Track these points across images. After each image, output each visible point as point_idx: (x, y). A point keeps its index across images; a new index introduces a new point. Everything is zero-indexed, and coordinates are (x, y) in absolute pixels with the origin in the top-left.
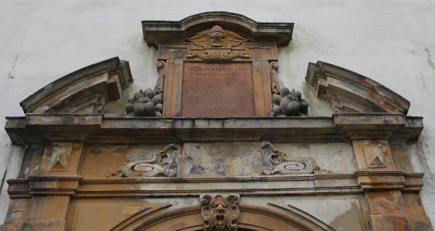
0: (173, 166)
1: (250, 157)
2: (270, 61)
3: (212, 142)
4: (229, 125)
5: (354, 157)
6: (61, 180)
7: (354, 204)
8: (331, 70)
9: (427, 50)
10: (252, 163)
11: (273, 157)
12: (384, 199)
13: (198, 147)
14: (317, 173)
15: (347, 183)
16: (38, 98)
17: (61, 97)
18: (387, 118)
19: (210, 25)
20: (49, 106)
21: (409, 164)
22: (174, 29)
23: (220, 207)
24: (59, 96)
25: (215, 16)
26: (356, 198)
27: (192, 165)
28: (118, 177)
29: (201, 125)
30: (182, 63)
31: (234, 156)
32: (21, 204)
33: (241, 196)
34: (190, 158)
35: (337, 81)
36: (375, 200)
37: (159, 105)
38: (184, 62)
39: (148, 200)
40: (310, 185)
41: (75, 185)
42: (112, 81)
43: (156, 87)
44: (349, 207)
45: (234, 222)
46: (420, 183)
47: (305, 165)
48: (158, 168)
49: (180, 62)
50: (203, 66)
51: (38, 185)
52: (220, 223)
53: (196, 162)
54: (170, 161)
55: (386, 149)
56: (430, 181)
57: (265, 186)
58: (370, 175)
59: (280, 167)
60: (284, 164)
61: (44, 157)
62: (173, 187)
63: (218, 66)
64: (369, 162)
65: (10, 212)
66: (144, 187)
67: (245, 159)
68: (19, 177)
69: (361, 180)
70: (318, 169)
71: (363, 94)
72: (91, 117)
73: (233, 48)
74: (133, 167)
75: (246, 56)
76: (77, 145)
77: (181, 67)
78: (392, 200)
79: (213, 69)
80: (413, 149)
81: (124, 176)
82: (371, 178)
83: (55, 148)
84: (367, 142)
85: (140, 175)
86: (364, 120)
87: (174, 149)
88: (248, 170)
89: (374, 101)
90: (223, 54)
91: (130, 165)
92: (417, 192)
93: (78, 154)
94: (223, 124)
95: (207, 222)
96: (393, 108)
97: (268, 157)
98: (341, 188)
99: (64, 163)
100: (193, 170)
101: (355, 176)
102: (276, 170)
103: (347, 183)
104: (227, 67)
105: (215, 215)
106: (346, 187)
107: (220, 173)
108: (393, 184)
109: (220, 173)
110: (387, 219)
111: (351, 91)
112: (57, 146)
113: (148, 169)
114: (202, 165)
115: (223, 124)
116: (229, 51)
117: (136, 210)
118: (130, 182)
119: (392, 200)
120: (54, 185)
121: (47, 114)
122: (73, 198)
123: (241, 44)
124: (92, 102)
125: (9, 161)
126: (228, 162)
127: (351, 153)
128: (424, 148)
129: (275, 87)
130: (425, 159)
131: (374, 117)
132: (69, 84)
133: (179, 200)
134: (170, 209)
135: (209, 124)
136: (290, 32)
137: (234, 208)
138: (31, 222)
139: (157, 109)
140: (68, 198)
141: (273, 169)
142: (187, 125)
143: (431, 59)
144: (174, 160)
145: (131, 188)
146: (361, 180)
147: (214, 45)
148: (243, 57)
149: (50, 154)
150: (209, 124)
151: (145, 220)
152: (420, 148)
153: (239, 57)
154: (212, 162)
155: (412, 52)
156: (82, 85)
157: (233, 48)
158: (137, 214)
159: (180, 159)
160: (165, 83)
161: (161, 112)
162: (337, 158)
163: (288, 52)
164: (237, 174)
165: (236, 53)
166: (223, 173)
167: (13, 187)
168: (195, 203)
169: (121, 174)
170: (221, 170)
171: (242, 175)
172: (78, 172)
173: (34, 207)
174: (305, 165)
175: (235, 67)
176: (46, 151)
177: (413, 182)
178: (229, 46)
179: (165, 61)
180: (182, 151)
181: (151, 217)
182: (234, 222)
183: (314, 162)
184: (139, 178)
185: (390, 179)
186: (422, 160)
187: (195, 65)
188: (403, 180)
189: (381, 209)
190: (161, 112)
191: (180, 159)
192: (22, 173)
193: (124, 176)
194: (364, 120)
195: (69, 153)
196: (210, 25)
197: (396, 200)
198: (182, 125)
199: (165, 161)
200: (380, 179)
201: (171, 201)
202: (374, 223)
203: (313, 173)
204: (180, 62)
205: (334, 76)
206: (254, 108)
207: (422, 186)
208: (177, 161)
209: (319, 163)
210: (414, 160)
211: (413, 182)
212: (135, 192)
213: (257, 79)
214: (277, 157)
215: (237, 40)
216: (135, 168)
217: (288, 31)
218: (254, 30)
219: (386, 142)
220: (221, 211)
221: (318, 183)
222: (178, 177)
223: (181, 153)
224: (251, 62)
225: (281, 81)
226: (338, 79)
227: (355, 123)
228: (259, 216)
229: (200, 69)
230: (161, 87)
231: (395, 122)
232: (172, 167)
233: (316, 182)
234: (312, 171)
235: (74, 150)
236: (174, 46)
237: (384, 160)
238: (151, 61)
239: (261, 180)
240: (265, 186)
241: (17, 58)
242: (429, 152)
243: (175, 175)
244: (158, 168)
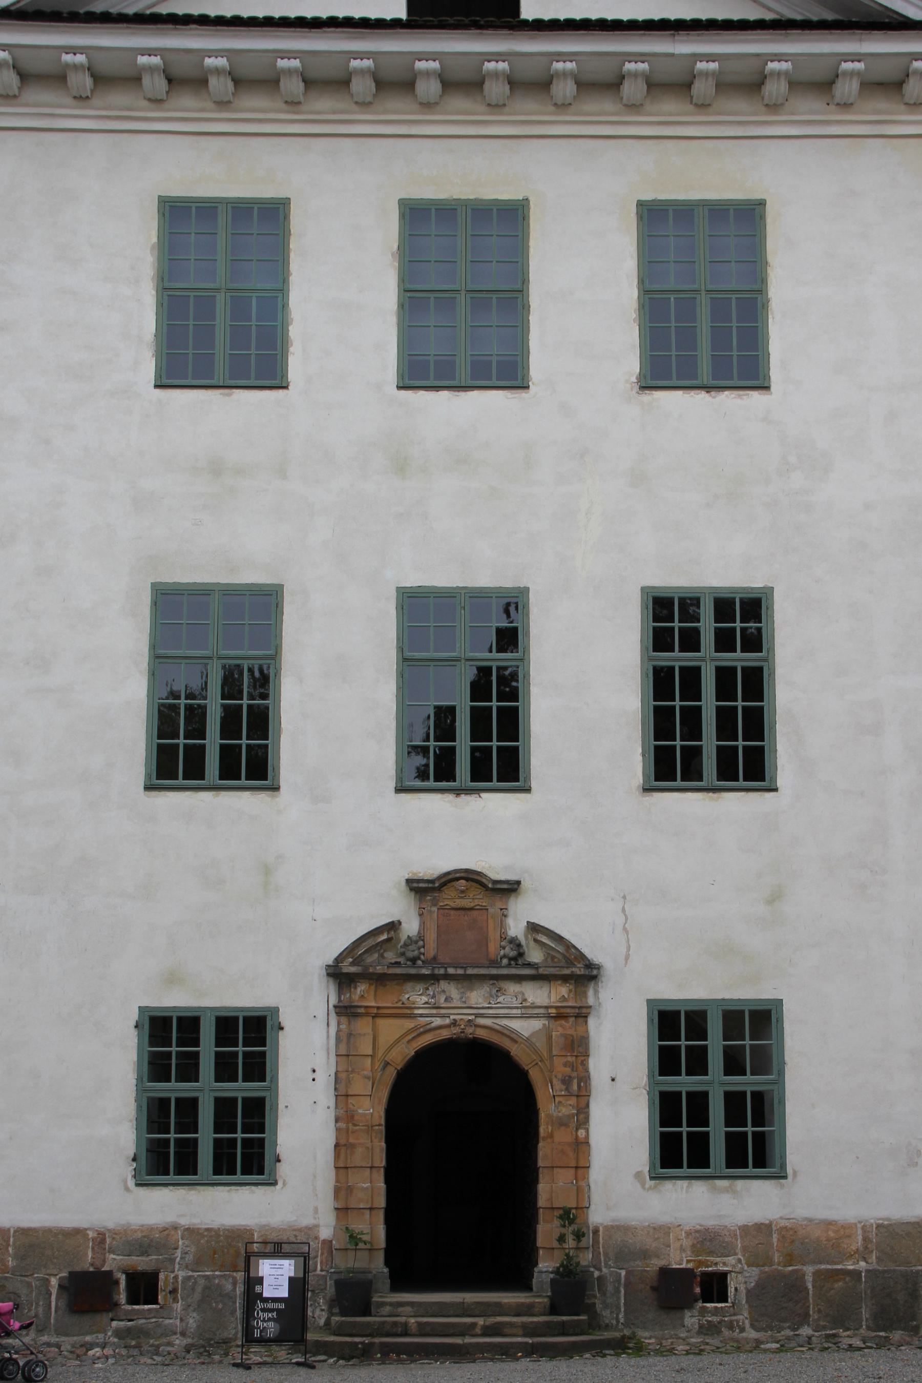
0: (433, 997)
1: (483, 990)
2: (501, 909)
3: (458, 980)
4: (470, 971)
5: (550, 992)
6: (366, 1007)
7: (544, 1025)
8: (541, 929)
9: (624, 897)
10: (484, 995)
11: (497, 991)
12: (563, 1022)
13: (449, 983)
14: (524, 1004)
15: (542, 1011)
16: (345, 953)
17: (358, 952)
18: (574, 969)
19: (458, 879)
20: (352, 958)
21: (586, 997)
22: (430, 885)
23: (462, 1027)
24: (357, 950)
25: (460, 873)
26: (547, 1020)
27: (445, 996)
28: (399, 1005)
29: (451, 971)
30: (436, 910)
31: (472, 990)
32: (344, 1019)
33: (476, 1017)
34: (444, 991)
35: (545, 937)
36: (558, 1022)
37: (422, 950)
38: (438, 909)
39: (419, 1018)
40: (519, 1011)
41: (375, 1011)
42: (390, 936)
43: (419, 932)
44: (541, 1026)
45: (470, 1034)
46: (588, 1012)
47: (517, 998)
48: (425, 999)
49: (435, 909)
50: (452, 912)
51: (353, 1010)
52: (462, 1035)
53: (448, 994)
54: (432, 993)
55: (571, 987)
56: (597, 1008)
57: (491, 1011)
58: (556, 1007)
59: (501, 999)
60: (504, 997)
61: (352, 990)
62: (434, 1011)
63: (463, 912)
64: (558, 998)
65: (339, 1024)
66: (416, 1012)
67: (479, 992)
68: (339, 1002)
69: (550, 1011)
70: (525, 1000)
71: (560, 949)
72: (380, 967)
73: (475, 897)
74: (409, 998)
75: (484, 904)
76: (371, 982)
77: (436, 914)
78: (568, 1022)
79: (459, 915)
80: (592, 985)
81: (403, 1004)
82: (557, 1010)
83: (358, 984)
84: (559, 982)
85: (414, 1004)
86: (557, 971)
87: (433, 984)
88: (480, 1000)
89: (568, 955)
90: (466, 903)
91: (407, 996)
92: (586, 1017)
93: (373, 987)
94: (465, 971)
95: (455, 1034)
96: (579, 963)
97: (494, 991)
98: (538, 1014)
99: (366, 995)
100: (446, 1000)
101: (547, 1007)
102: (498, 1001)
103: (542, 1011)
104: (469, 913)
105: (460, 1031)
106: (541, 1014)
107: (463, 1002)
108: (570, 1013)
109: (463, 1002)
110: (562, 1035)
111: (554, 946)
112: (359, 982)
113: (418, 1000)
114: (452, 996)
115: (465, 971)
116: (471, 900)
117: (412, 1025)
118: (407, 1008)
119: (568, 1022)
120: (362, 1010)
121: (353, 964)
122: (373, 1017)
123: (481, 893)
124: (377, 949)
125: (328, 986)
126: (468, 994)
127: (548, 989)
128: (600, 984)
129: (504, 933)
130: (598, 992)
131: (565, 969)
132: (363, 942)
133: (438, 1019)
134: (433, 1025)
135: (456, 971)
136: (502, 965)
137: (471, 1026)
138: (353, 1032)
139: (421, 953)
140: (371, 1018)
141: (497, 1000)
142: (442, 971)
143: (625, 906)
144: (434, 992)
145: (409, 1012)
146: (550, 1011)
147: (460, 895)
148: (482, 906)
149: (355, 988)
150: (456, 971)
151: (418, 1032)
152: (597, 984)
153: (478, 905)
154: (458, 994)
155: (612, 900)
156: (371, 942)
157: (475, 897)
158: (413, 1028)
159: (438, 992)
160: (425, 930)
161: (424, 954)
162: (539, 992)
163: (517, 897)
164: (473, 1003)
165: (476, 902)
166: (465, 1002)
167: (338, 1009)
168: (447, 1021)
169: (401, 1003)
170: (464, 999)
171: (477, 1004)
172: (375, 999)
173: (353, 1023)
174: (517, 998)
175: (475, 913)
176: (352, 985)
177: (584, 1011)
178: (471, 896)
179: (424, 909)
180: (438, 986)
181: (422, 1030)
182: (470, 1034)
183: (523, 994)
184: (413, 1006)
185: (568, 1010)
186: (596, 992)
187: (446, 911)
188: (577, 1011)
189: (560, 1029)
190: (424, 954)
191: (438, 992)
192: (340, 1001)
193: (403, 1004)
194: (557, 971)
195: (367, 988)
196: (458, 879)
197: (571, 1023)
198: (439, 971)
199: (428, 992)
200: (562, 1010)
201: (433, 1019)
202: (553, 1037)
203: (521, 1004)
204: (435, 909)
205: (543, 933)
206: (487, 950)
207: (589, 1013)
208: (436, 993)
209: (526, 996)
210: (591, 993)
211: (584, 1011)
212: (411, 1014)
213: (491, 922)
214: (499, 990)
215: (477, 890)
216: (410, 999)
217: (516, 886)
218: (490, 886)
219: (573, 982)
220: (463, 1029)
221: (524, 1011)
222: (436, 1005)
223: (438, 988)
224: (487, 909)
225: (509, 925)
226: (547, 936)
227: (552, 973)
228: (486, 1030)
229: (450, 915)
230: (422, 932)
231: (579, 973)
232: (432, 998)
233: (523, 1010)
234: (520, 1002)
235: (370, 984)
236: (430, 894)
237: (568, 996)
238: (413, 904)
239: (489, 1008)
240: (491, 1011)
241: (314, 901)
242: (602, 987)
243: (435, 1004)
244: (425, 999)
